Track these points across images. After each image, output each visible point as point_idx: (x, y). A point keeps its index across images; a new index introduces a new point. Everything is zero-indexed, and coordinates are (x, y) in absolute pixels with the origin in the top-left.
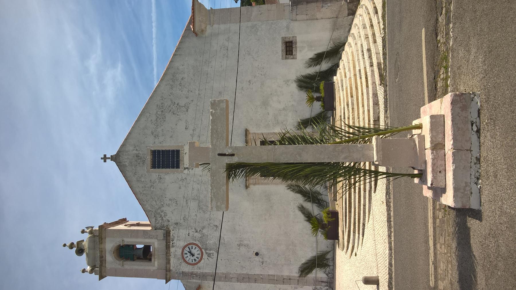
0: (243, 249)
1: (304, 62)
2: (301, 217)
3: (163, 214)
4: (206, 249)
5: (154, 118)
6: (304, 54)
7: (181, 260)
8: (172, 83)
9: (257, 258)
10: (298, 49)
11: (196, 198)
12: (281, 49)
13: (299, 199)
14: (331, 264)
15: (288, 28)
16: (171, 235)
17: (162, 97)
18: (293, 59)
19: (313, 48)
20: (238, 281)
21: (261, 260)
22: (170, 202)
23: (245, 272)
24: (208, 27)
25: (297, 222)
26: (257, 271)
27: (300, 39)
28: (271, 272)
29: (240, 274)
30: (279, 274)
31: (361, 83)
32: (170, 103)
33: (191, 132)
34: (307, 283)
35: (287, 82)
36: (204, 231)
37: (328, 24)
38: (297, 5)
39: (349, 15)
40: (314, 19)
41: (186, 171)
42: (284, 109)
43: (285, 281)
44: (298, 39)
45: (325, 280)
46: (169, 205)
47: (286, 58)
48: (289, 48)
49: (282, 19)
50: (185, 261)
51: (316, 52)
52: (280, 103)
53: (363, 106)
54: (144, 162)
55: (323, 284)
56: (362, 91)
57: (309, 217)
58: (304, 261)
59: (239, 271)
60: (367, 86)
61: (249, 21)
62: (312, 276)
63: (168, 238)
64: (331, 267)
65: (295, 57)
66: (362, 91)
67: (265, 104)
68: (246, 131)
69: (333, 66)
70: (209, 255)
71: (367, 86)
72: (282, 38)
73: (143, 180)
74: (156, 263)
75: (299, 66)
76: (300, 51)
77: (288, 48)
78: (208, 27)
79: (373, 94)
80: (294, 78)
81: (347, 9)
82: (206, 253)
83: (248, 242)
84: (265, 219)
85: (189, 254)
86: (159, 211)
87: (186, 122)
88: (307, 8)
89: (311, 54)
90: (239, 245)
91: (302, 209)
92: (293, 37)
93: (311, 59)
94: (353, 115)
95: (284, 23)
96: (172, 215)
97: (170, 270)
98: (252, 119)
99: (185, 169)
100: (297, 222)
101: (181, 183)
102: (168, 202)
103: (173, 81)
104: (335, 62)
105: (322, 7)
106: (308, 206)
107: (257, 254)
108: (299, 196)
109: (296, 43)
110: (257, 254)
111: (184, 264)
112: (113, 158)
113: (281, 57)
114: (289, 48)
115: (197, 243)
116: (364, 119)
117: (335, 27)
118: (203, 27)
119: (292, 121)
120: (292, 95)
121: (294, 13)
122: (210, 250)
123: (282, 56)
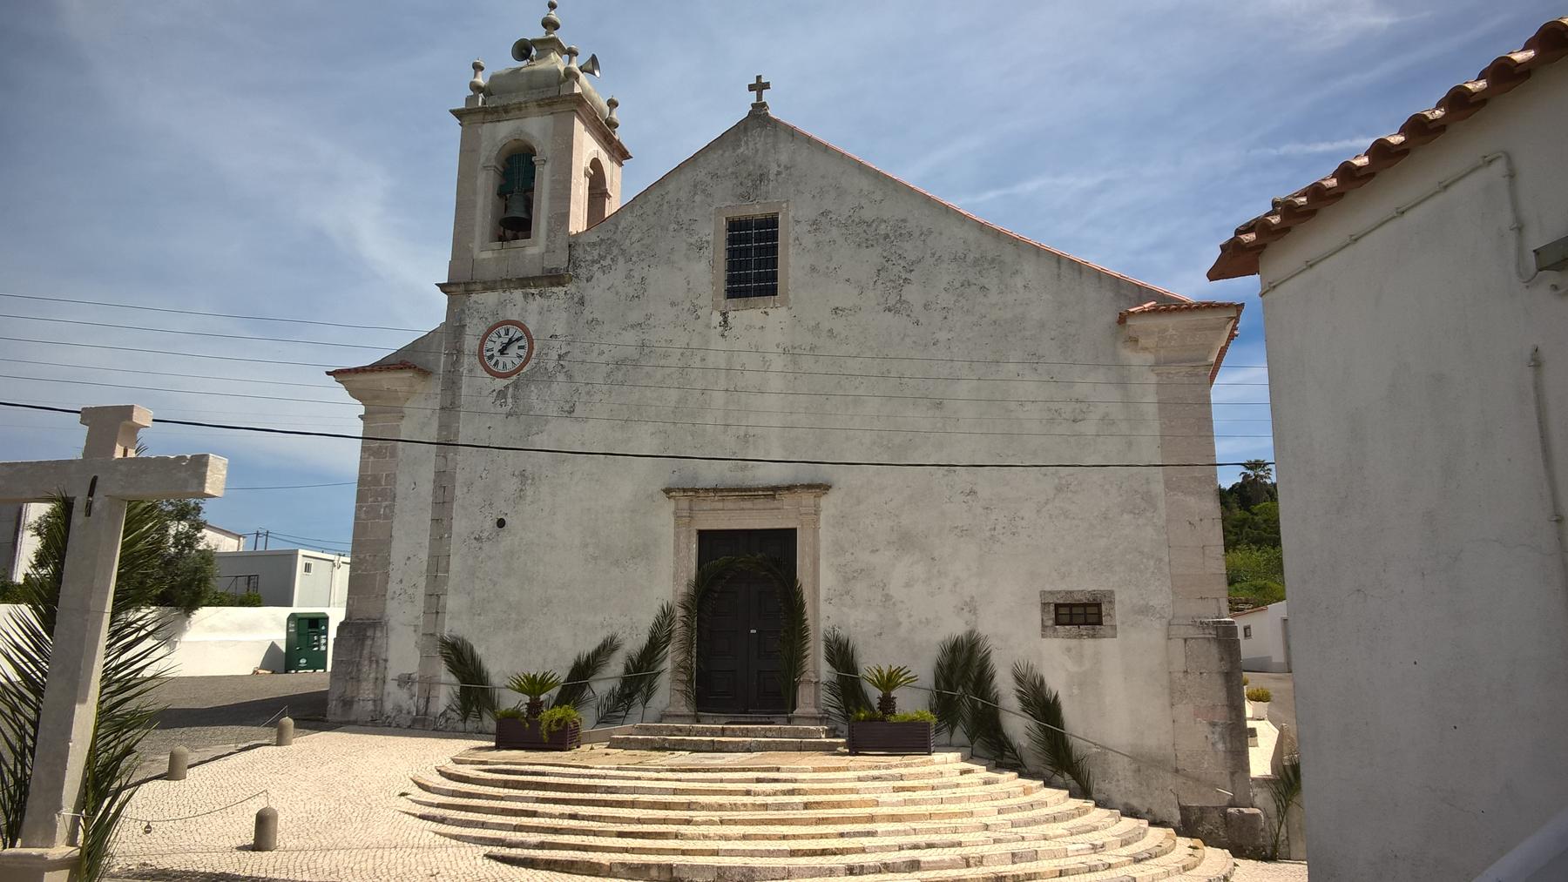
0: (511, 485)
2: (588, 646)
3: (608, 261)
4: (516, 385)
10: (1074, 642)
13: (634, 642)
14: (470, 725)
15: (1145, 610)
21: (486, 534)
23: (458, 492)
26: (460, 525)
28: (455, 563)
34: (426, 657)
35: (971, 606)
36: (561, 377)
40: (1175, 694)
41: (717, 318)
42: (888, 597)
45: (432, 709)
55: (422, 702)
58: (479, 651)
59: (460, 477)
62: (443, 673)
64: (460, 726)
67: (905, 541)
70: (502, 394)
80: (984, 629)
84: (586, 546)
89: (1056, 684)
90: (523, 474)
91: (607, 648)
97: (468, 292)
106: (615, 668)
107: (501, 523)
109: (1093, 636)
110: (501, 523)
112: (759, 109)
113: (1048, 588)
115: (532, 362)
118: (1149, 342)
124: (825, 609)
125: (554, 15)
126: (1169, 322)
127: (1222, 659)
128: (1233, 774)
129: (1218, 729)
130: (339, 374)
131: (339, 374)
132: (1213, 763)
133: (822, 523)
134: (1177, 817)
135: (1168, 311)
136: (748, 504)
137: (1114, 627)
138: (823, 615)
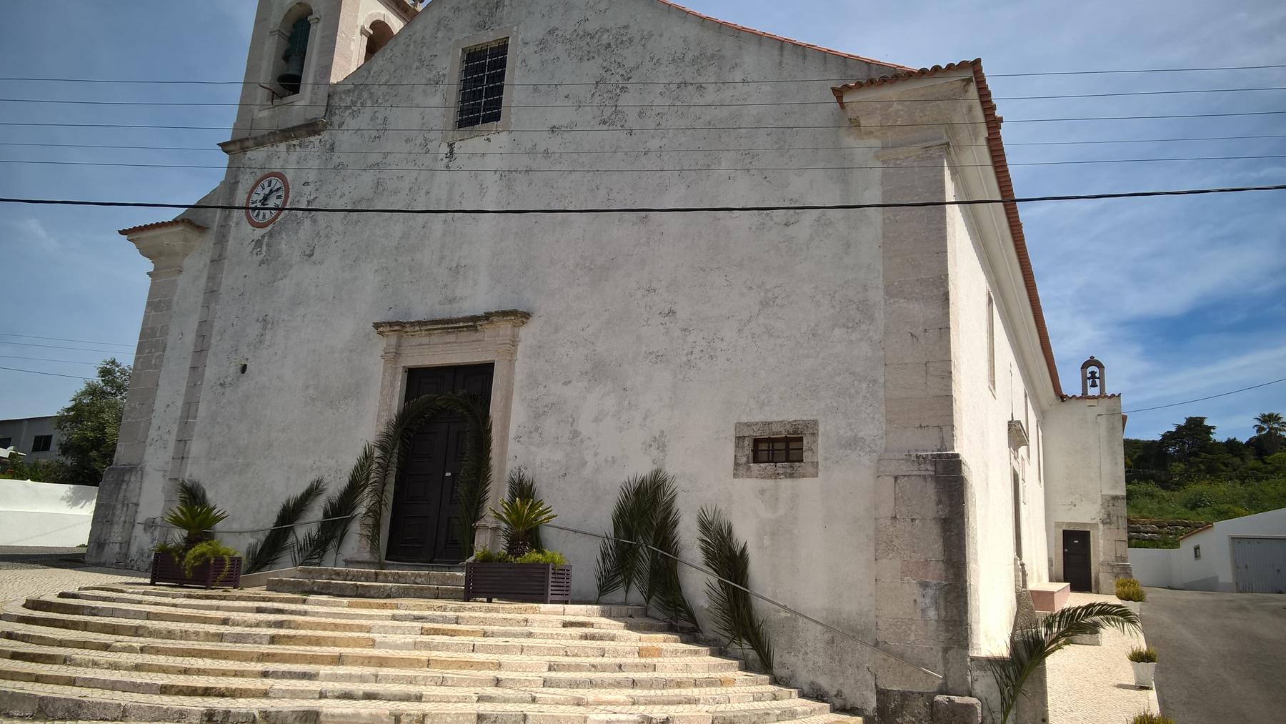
0: (254, 331)
1: (722, 506)
2: (298, 491)
4: (271, 234)
5: (591, 27)
6: (749, 504)
7: (259, 174)
8: (690, 55)
9: (234, 369)
10: (769, 483)
11: (381, 188)
12: (774, 418)
13: (335, 486)
15: (853, 443)
16: (312, 139)
17: (651, 34)
18: (737, 465)
19: (767, 542)
20: (202, 323)
22: (380, 116)
24: (875, 143)
25: (288, 478)
26: (211, 372)
27: (803, 491)
29: (212, 327)
30: (196, 429)
31: (224, 673)
32: (630, 63)
33: (542, 146)
35: (660, 443)
37: (853, 606)
38: (936, 478)
39: (882, 694)
40: (882, 545)
42: (576, 434)
43: (182, 444)
44: (805, 484)
46: (373, 118)
47: (740, 439)
48: (777, 450)
49: (889, 421)
50: (256, 185)
51: (752, 553)
52: (597, 420)
53: (138, 668)
54: (482, 26)
56: (199, 672)
57: (291, 514)
59: (217, 325)
60: (165, 690)
61: (889, 292)
63: (303, 132)
65: (742, 471)
66: (199, 672)
67: (598, 371)
68: (520, 316)
69: (691, 616)
71: (165, 690)
72: (815, 422)
73: (440, 34)
74: (264, 116)
75: (712, 487)
76: (762, 492)
77: (782, 446)
78: (875, 143)
79: (79, 704)
81: (907, 688)
82: (263, 237)
83: (267, 343)
84: (307, 387)
85: (267, 191)
86: (365, 95)
87: (570, 128)
88: (923, 519)
89: (744, 535)
91: (313, 492)
92: (815, 465)
93: (730, 532)
94: (197, 633)
95: (871, 429)
96: (349, 133)
97: (244, 150)
98: (556, 331)
99: (451, 146)
100: (288, 478)
101: (420, 140)
102: (380, 116)
103: (695, 60)
104: (710, 627)
105: (924, 585)
108: (345, 482)
109: (791, 476)
111: (251, 182)
113: (744, 419)
114: (777, 450)
116: (95, 664)
117: (842, 634)
119: (538, 463)
120: (614, 460)
121: (905, 468)
122: (269, 245)
123: (748, 425)
124: (513, 448)
127: (939, 502)
128: (946, 650)
129: (930, 591)
130: (123, 232)
133: (519, 355)
136: (451, 338)
138: (510, 454)
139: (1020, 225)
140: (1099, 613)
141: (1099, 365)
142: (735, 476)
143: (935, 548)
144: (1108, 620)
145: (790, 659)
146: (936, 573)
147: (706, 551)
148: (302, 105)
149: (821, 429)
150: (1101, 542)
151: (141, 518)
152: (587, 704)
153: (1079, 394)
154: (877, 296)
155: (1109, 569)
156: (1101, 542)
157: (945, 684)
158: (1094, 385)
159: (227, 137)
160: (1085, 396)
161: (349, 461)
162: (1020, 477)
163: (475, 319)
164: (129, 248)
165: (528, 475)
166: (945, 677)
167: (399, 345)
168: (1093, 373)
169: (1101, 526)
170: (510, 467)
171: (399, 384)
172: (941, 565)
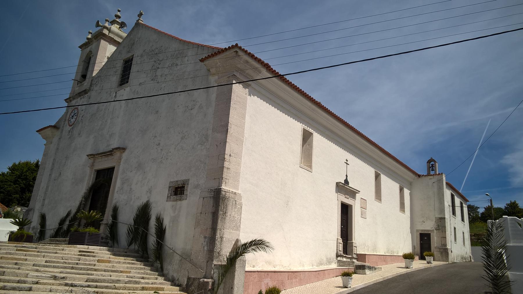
4: (73, 128)
10: (174, 203)
13: (74, 211)
15: (197, 187)
18: (168, 197)
35: (150, 191)
40: (197, 224)
42: (131, 189)
52: (137, 184)
54: (129, 52)
63: (83, 93)
67: (140, 166)
89: (166, 223)
99: (116, 93)
105: (205, 237)
109: (180, 200)
113: (172, 180)
117: (186, 257)
123: (172, 182)
124: (116, 195)
125: (119, 14)
126: (216, 60)
127: (213, 206)
128: (207, 262)
129: (206, 240)
130: (37, 131)
131: (37, 131)
132: (201, 258)
133: (122, 163)
134: (184, 282)
135: (213, 55)
136: (106, 159)
137: (187, 195)
138: (115, 198)
139: (319, 103)
140: (254, 245)
141: (435, 161)
142: (167, 201)
143: (209, 222)
144: (258, 247)
145: (169, 267)
146: (208, 233)
147: (156, 228)
148: (86, 84)
149: (190, 182)
150: (435, 238)
151: (31, 227)
152: (40, 271)
153: (425, 174)
154: (210, 132)
155: (438, 250)
156: (435, 238)
157: (206, 275)
158: (433, 170)
159: (67, 96)
160: (429, 175)
161: (77, 203)
162: (451, 213)
163: (111, 151)
164: (39, 136)
165: (118, 204)
166: (206, 272)
167: (94, 162)
168: (432, 165)
169: (435, 231)
170: (114, 202)
171: (93, 176)
172: (210, 230)
